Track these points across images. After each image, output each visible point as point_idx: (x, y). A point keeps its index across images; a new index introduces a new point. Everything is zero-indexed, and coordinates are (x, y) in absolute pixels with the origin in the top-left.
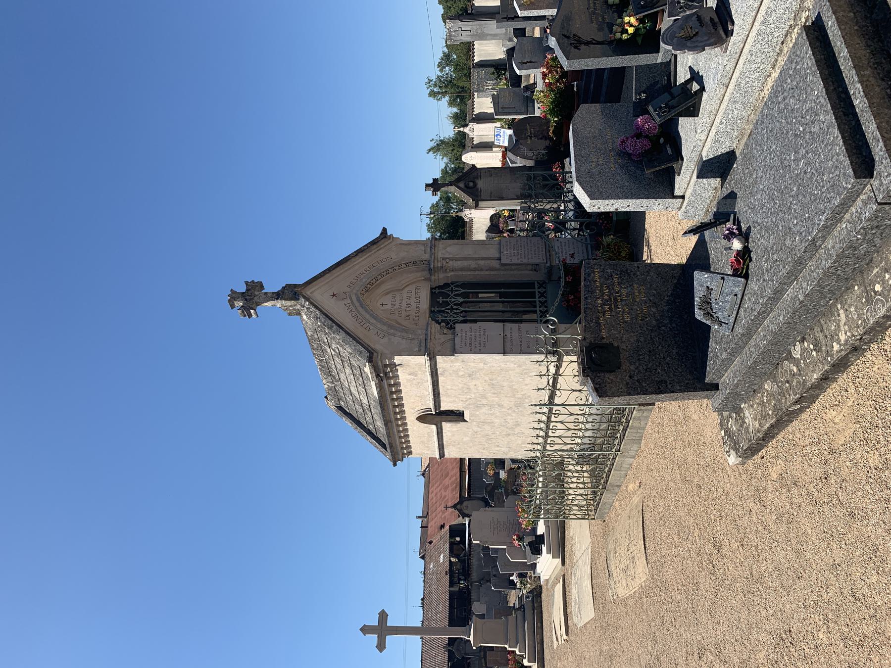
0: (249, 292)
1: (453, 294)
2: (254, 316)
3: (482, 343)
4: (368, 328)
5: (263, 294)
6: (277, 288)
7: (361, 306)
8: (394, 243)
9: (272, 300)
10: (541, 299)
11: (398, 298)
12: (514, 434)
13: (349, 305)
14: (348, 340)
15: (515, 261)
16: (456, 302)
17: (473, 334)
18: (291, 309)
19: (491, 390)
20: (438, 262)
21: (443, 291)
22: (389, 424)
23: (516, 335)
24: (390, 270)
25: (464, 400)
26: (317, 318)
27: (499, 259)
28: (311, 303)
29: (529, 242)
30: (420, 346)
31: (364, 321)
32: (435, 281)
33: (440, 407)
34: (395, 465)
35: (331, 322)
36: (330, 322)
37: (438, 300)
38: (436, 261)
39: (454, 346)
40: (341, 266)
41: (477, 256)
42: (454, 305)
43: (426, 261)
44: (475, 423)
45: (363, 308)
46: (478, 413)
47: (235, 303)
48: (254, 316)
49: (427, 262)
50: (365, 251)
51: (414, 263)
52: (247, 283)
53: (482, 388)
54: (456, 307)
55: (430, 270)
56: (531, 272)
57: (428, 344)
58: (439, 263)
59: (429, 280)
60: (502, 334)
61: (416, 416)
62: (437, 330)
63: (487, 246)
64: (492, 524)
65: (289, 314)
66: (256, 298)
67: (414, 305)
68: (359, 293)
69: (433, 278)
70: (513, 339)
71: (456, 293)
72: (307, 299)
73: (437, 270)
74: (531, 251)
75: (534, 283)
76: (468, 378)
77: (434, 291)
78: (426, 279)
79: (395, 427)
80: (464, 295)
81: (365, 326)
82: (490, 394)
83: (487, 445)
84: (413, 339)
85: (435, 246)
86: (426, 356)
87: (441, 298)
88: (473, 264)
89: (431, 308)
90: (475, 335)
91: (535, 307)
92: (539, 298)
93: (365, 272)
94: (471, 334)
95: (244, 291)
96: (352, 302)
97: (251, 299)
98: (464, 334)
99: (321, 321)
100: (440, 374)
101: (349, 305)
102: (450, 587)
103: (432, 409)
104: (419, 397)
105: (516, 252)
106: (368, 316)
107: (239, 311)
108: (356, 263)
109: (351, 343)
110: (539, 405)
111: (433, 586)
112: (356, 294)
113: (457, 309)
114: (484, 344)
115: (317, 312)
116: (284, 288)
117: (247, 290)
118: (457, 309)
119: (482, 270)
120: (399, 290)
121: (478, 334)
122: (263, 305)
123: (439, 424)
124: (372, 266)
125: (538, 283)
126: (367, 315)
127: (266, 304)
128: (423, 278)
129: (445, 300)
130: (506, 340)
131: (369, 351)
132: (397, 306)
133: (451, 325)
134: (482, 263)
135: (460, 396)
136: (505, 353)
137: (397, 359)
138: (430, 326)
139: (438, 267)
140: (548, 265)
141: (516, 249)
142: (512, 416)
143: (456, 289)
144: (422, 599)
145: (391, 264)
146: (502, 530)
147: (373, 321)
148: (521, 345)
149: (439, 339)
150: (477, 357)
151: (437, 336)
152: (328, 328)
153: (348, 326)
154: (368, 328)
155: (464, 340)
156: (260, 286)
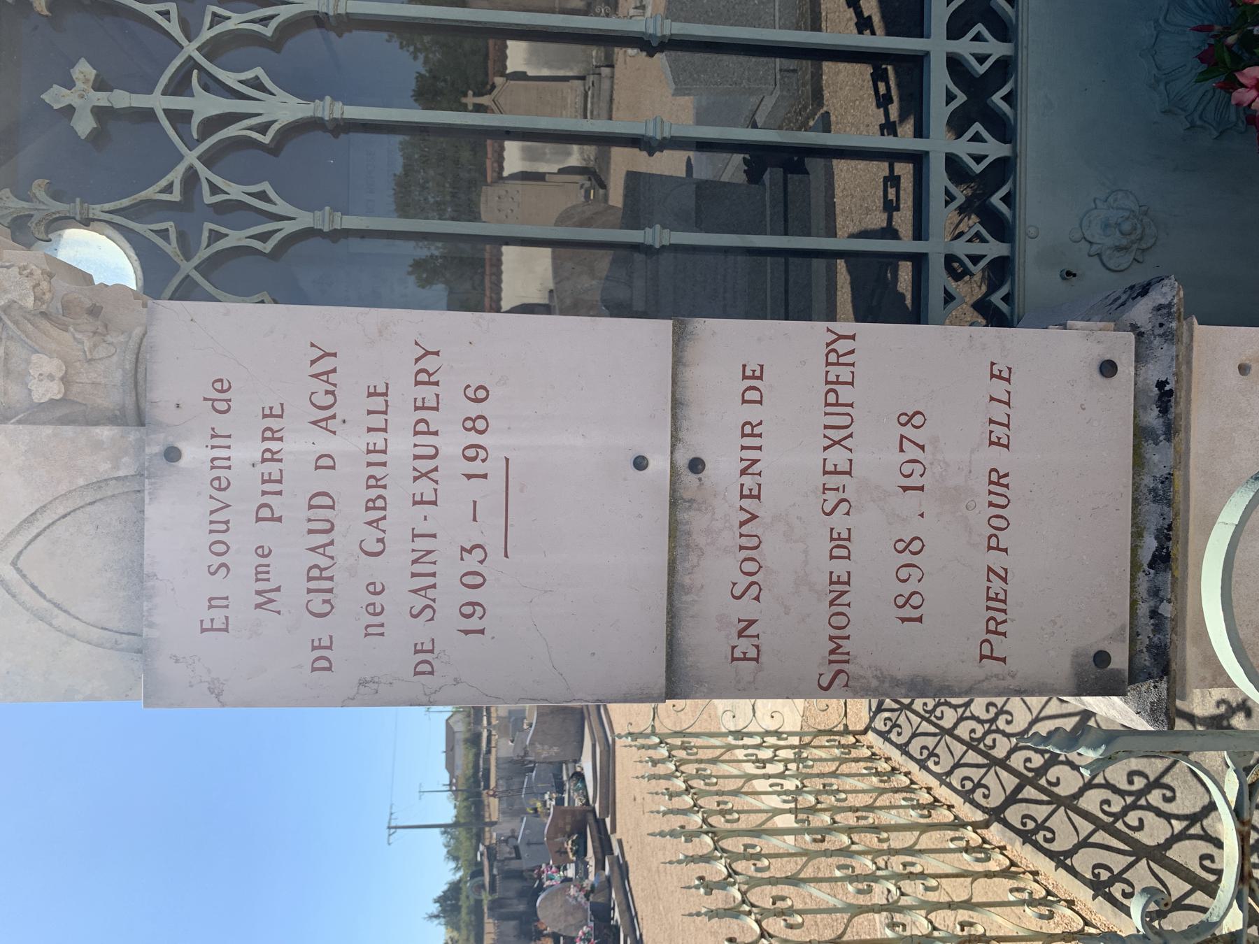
3: (449, 570)
10: (965, 47)
37: (57, 97)
42: (209, 160)
60: (659, 464)
87: (84, 71)
94: (326, 444)
98: (245, 452)
114: (473, 424)
121: (401, 445)
129: (122, 99)
130: (696, 521)
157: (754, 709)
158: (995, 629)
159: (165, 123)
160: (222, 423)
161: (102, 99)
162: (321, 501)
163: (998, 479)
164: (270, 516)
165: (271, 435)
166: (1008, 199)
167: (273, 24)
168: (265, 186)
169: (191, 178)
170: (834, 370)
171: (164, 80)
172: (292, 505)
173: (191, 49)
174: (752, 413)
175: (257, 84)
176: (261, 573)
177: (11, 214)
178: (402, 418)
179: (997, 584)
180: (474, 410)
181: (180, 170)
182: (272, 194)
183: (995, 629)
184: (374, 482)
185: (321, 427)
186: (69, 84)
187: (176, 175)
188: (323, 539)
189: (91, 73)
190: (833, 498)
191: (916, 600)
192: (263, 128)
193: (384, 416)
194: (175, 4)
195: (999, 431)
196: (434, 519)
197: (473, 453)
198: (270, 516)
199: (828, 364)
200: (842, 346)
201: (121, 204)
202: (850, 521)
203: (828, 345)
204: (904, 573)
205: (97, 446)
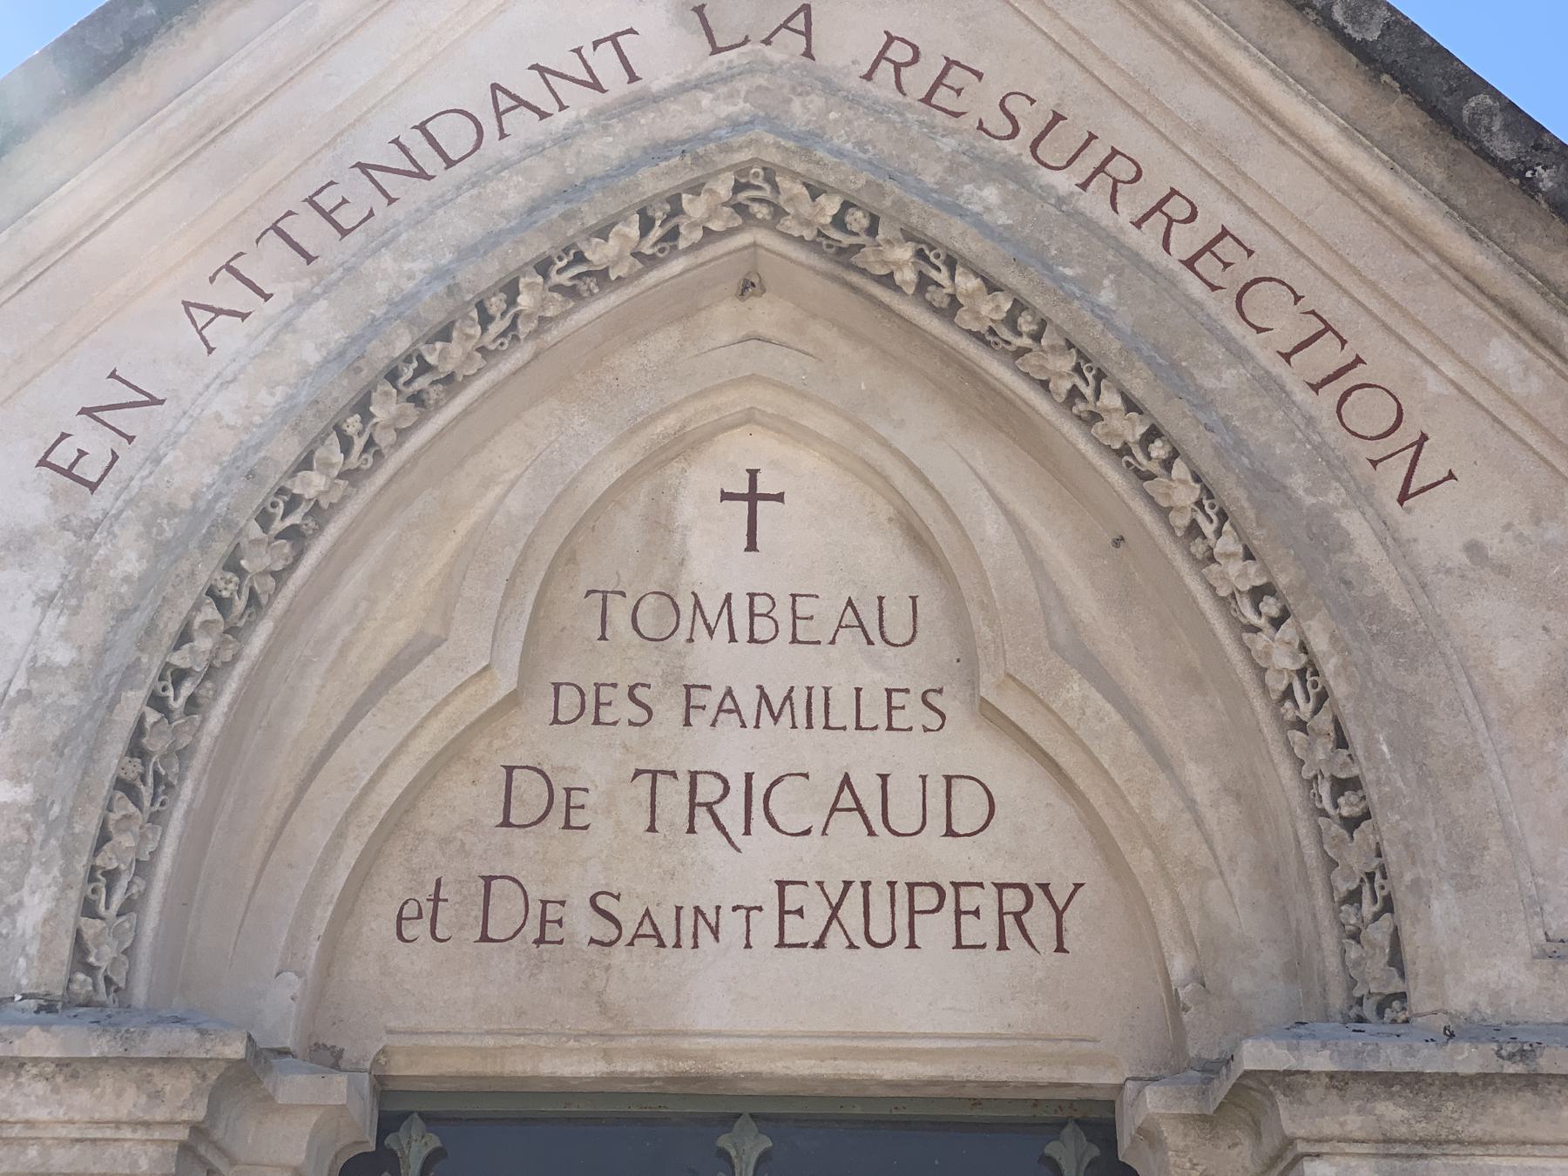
4: (239, 297)
38: (1393, 1113)
49: (1376, 977)
51: (1342, 786)
79: (165, 865)
108: (1259, 78)
124: (1245, 270)
126: (419, 266)
128: (1179, 966)
157: (812, 596)
164: (1164, 209)
170: (985, 900)
177: (402, 1149)
185: (641, 924)
193: (852, 724)
198: (1164, 209)
199: (1000, 887)
203: (1044, 887)
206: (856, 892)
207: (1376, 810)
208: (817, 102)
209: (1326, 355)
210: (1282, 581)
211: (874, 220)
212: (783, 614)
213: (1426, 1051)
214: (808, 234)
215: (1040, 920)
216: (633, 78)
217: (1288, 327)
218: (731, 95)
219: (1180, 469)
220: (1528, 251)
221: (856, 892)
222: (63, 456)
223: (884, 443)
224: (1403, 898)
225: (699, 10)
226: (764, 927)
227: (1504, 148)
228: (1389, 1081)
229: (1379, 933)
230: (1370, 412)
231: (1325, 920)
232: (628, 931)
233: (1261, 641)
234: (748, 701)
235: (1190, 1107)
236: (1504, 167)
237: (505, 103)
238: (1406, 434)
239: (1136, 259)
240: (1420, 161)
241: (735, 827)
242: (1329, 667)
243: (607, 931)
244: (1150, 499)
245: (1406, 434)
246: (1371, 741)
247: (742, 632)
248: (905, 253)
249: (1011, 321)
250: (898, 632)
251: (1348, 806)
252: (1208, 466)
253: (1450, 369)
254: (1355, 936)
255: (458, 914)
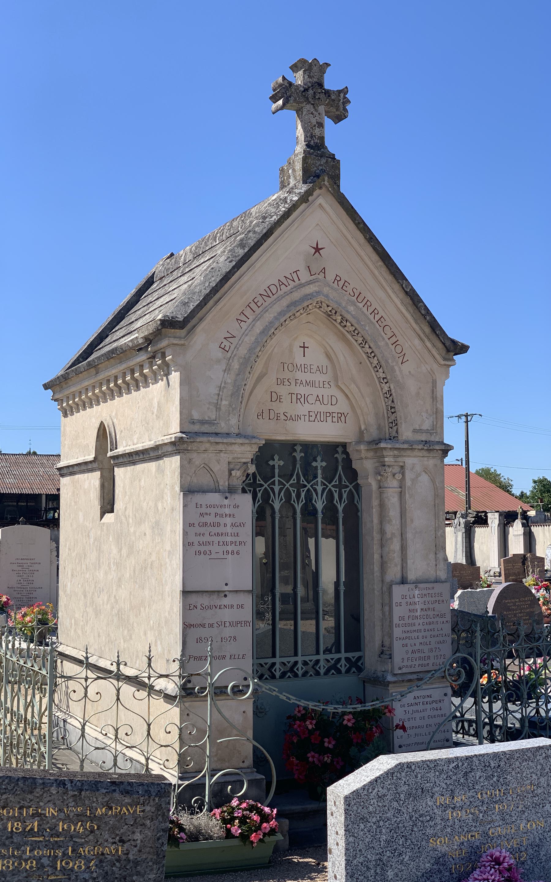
0: (322, 96)
1: (333, 489)
2: (274, 106)
3: (206, 548)
4: (244, 319)
5: (319, 120)
6: (331, 145)
7: (294, 304)
8: (435, 366)
9: (306, 137)
10: (343, 662)
11: (318, 378)
12: (86, 606)
13: (296, 279)
14: (213, 279)
15: (397, 612)
16: (272, 494)
17: (229, 529)
18: (290, 171)
19: (138, 565)
20: (395, 456)
21: (340, 468)
22: (93, 371)
23: (227, 615)
24: (375, 362)
25: (127, 513)
26: (264, 218)
27: (403, 581)
28: (294, 207)
29: (441, 639)
30: (202, 422)
31: (258, 311)
32: (357, 451)
33: (119, 465)
34: (46, 387)
35: (252, 244)
36: (252, 243)
38: (396, 452)
39: (203, 492)
40: (381, 263)
41: (409, 536)
43: (397, 432)
44: (99, 533)
45: (288, 307)
46: (111, 539)
47: (301, 72)
48: (274, 106)
49: (394, 434)
50: (417, 311)
52: (345, 91)
53: (141, 548)
54: (303, 495)
55: (378, 441)
56: (378, 643)
57: (204, 439)
58: (392, 460)
59: (360, 441)
60: (226, 588)
61: (106, 420)
62: (239, 456)
63: (432, 556)
64: (29, 561)
65: (282, 170)
66: (309, 107)
67: (302, 409)
68: (322, 298)
69: (362, 447)
70: (218, 609)
71: (336, 496)
72: (305, 198)
73: (378, 454)
74: (421, 643)
75: (360, 651)
76: (154, 520)
77: (340, 450)
78: (361, 433)
80: (330, 509)
81: (248, 312)
82: (133, 563)
83: (74, 554)
84: (218, 408)
85: (429, 450)
86: (180, 435)
88: (393, 528)
89: (301, 445)
90: (227, 534)
91: (328, 651)
92: (347, 659)
93: (371, 310)
95: (326, 87)
96: (302, 286)
97: (307, 98)
98: (227, 511)
99: (257, 225)
100: (159, 464)
101: (296, 279)
102: (47, 495)
103: (115, 451)
104: (131, 424)
105: (418, 614)
106: (269, 316)
107: (280, 80)
108: (390, 291)
109: (207, 285)
110: (118, 660)
111: (42, 470)
112: (318, 293)
113: (298, 496)
114: (233, 552)
115: (275, 217)
116: (333, 157)
117: (328, 93)
118: (298, 496)
119: (382, 546)
120: (336, 379)
121: (229, 539)
122: (299, 121)
123: (95, 465)
125: (359, 658)
126: (272, 316)
127: (300, 127)
129: (277, 471)
130: (215, 596)
131: (187, 320)
132: (300, 376)
133: (305, 486)
134: (396, 545)
135: (131, 504)
136: (185, 593)
137: (175, 377)
138: (247, 441)
139: (383, 457)
140: (390, 678)
141: (424, 613)
142: (107, 604)
143: (345, 496)
144: (35, 453)
145: (387, 362)
146: (20, 578)
147: (259, 327)
148: (203, 626)
149: (218, 461)
150: (178, 538)
151: (225, 458)
152: (241, 240)
153: (245, 278)
154: (244, 319)
155: (213, 511)
156: (338, 118)
158: (195, 658)
159: (272, 480)
160: (232, 507)
161: (276, 467)
162: (219, 525)
163: (224, 657)
165: (230, 516)
166: (266, 679)
167: (293, 503)
168: (261, 502)
169: (262, 485)
171: (281, 480)
172: (218, 519)
173: (288, 485)
174: (235, 607)
175: (281, 499)
176: (206, 514)
178: (234, 539)
179: (204, 658)
180: (235, 553)
181: (263, 483)
182: (259, 503)
183: (195, 658)
184: (222, 534)
186: (279, 460)
187: (262, 482)
188: (212, 525)
189: (281, 465)
190: (220, 624)
191: (201, 641)
192: (272, 501)
194: (328, 788)
195: (233, 657)
196: (216, 545)
197: (228, 552)
200: (248, 624)
201: (406, 757)
202: (215, 627)
204: (206, 639)
205: (225, 482)
206: (319, 413)
207: (397, 412)
208: (328, 288)
209: (394, 339)
210: (388, 378)
211: (336, 312)
212: (309, 368)
213: (401, 445)
214: (324, 311)
215: (343, 417)
216: (299, 280)
217: (390, 334)
218: (315, 286)
219: (375, 358)
220: (422, 326)
221: (319, 413)
222: (223, 346)
223: (327, 343)
224: (399, 424)
225: (308, 267)
226: (307, 417)
227: (423, 312)
228: (396, 449)
229: (395, 428)
230: (399, 349)
231: (387, 425)
232: (289, 418)
233: (383, 385)
234: (304, 382)
235: (366, 448)
236: (423, 315)
237: (281, 283)
238: (403, 353)
239: (369, 319)
240: (410, 309)
241: (303, 402)
242: (393, 391)
243: (286, 418)
244: (370, 361)
245: (403, 353)
246: (397, 403)
247: (303, 371)
248: (340, 318)
249: (354, 331)
250: (325, 372)
251: (393, 410)
252: (380, 359)
253: (409, 343)
254: (392, 428)
255: (266, 415)
